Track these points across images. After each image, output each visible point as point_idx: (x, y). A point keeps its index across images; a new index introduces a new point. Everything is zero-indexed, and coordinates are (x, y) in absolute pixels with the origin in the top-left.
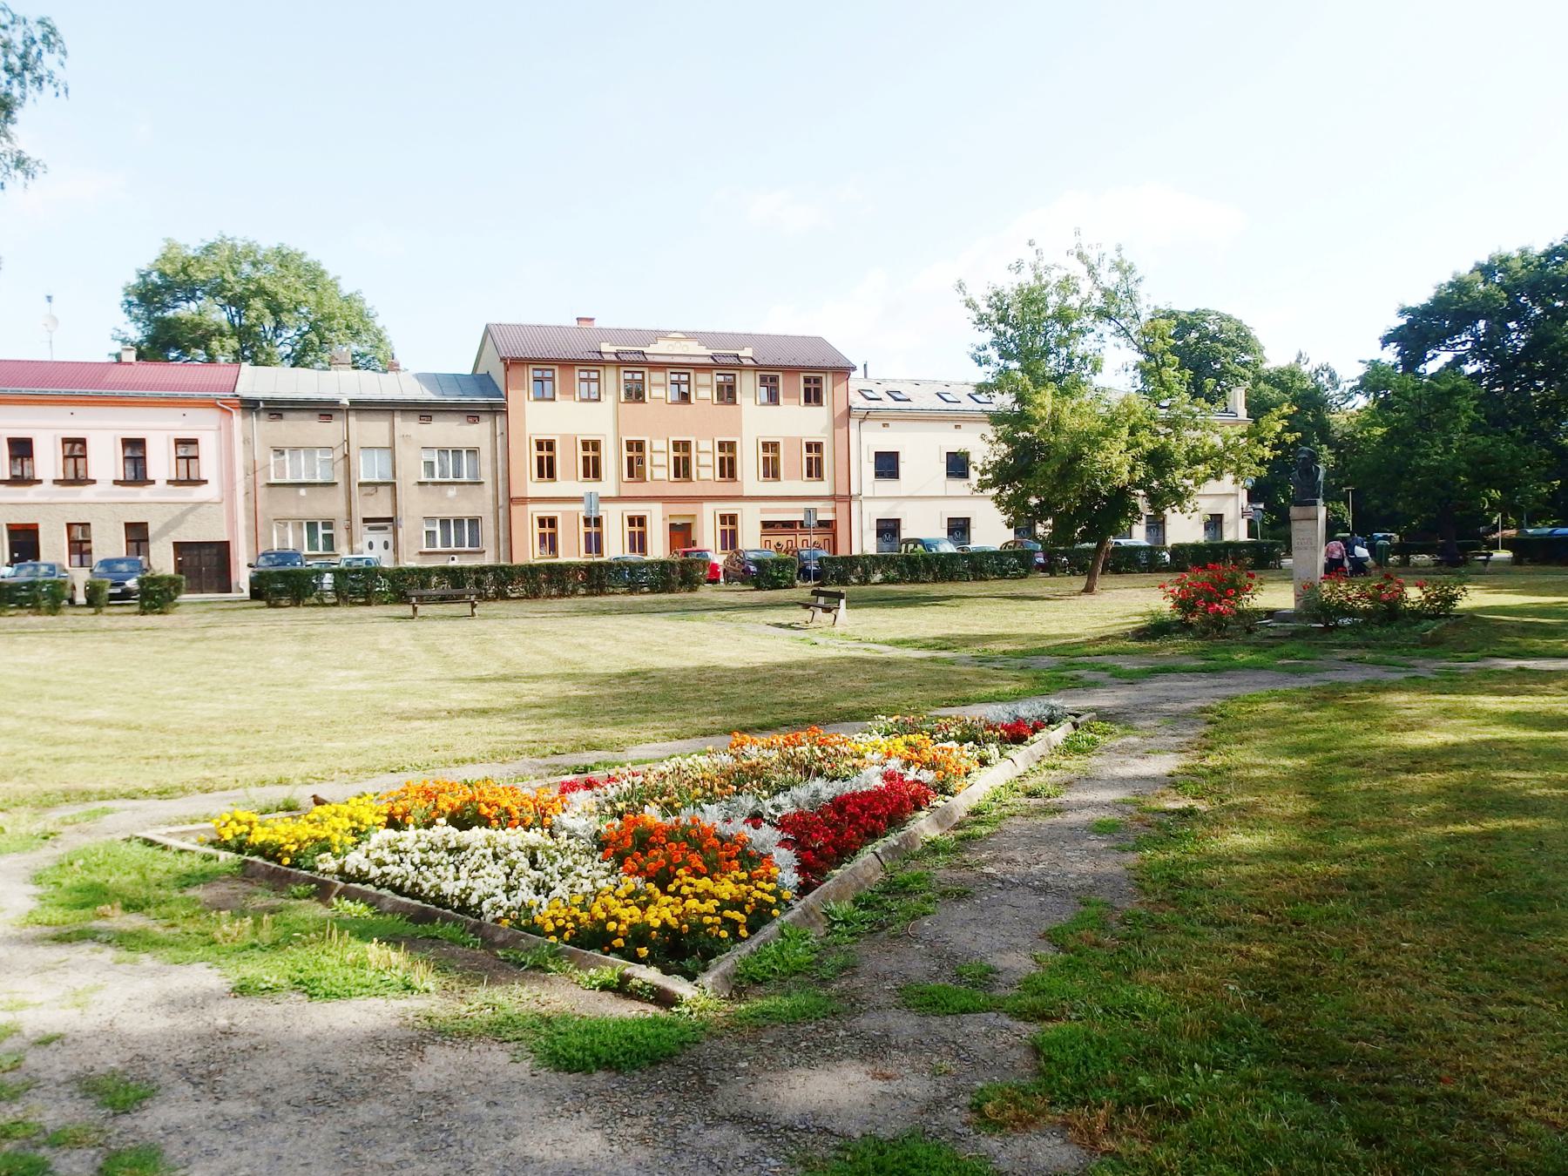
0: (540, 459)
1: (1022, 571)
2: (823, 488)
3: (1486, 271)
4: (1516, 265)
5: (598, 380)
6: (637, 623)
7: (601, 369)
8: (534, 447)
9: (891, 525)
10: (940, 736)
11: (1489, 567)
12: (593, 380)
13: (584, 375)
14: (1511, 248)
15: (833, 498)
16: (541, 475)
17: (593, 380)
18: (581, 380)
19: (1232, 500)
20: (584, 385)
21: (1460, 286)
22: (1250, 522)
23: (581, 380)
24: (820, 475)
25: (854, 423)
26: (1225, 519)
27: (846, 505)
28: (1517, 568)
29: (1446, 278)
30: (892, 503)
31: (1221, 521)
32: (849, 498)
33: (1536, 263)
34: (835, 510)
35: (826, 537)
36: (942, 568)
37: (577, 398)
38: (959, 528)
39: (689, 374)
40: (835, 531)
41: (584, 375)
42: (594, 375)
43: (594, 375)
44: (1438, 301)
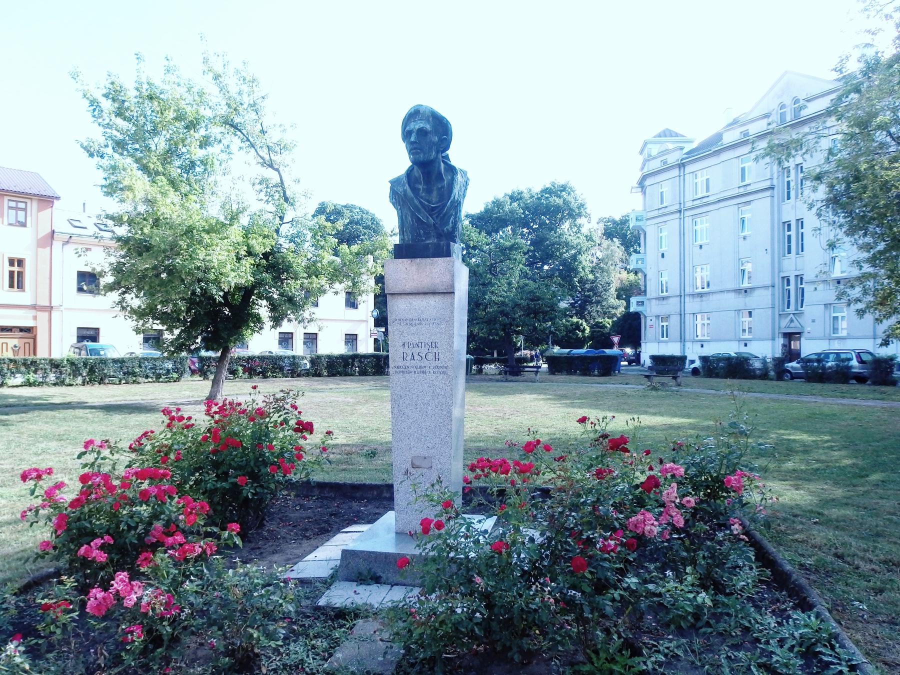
0: (11, 274)
1: (175, 375)
2: (24, 297)
3: (513, 198)
4: (526, 195)
5: (25, 210)
6: (49, 428)
7: (29, 201)
8: (7, 263)
9: (92, 333)
10: (535, 512)
11: (539, 375)
12: (21, 209)
13: (13, 204)
14: (523, 188)
15: (34, 307)
16: (11, 286)
17: (21, 209)
18: (10, 208)
19: (364, 324)
20: (13, 212)
21: (498, 204)
22: (375, 340)
23: (10, 208)
24: (21, 286)
25: (57, 245)
26: (359, 338)
27: (46, 314)
28: (552, 377)
29: (490, 199)
30: (350, 324)
31: (356, 339)
32: (49, 309)
33: (536, 197)
34: (35, 318)
35: (26, 340)
36: (92, 371)
37: (6, 222)
38: (89, 335)
39: (26, 203)
40: (35, 336)
41: (13, 204)
42: (22, 205)
43: (22, 205)
44: (487, 211)
